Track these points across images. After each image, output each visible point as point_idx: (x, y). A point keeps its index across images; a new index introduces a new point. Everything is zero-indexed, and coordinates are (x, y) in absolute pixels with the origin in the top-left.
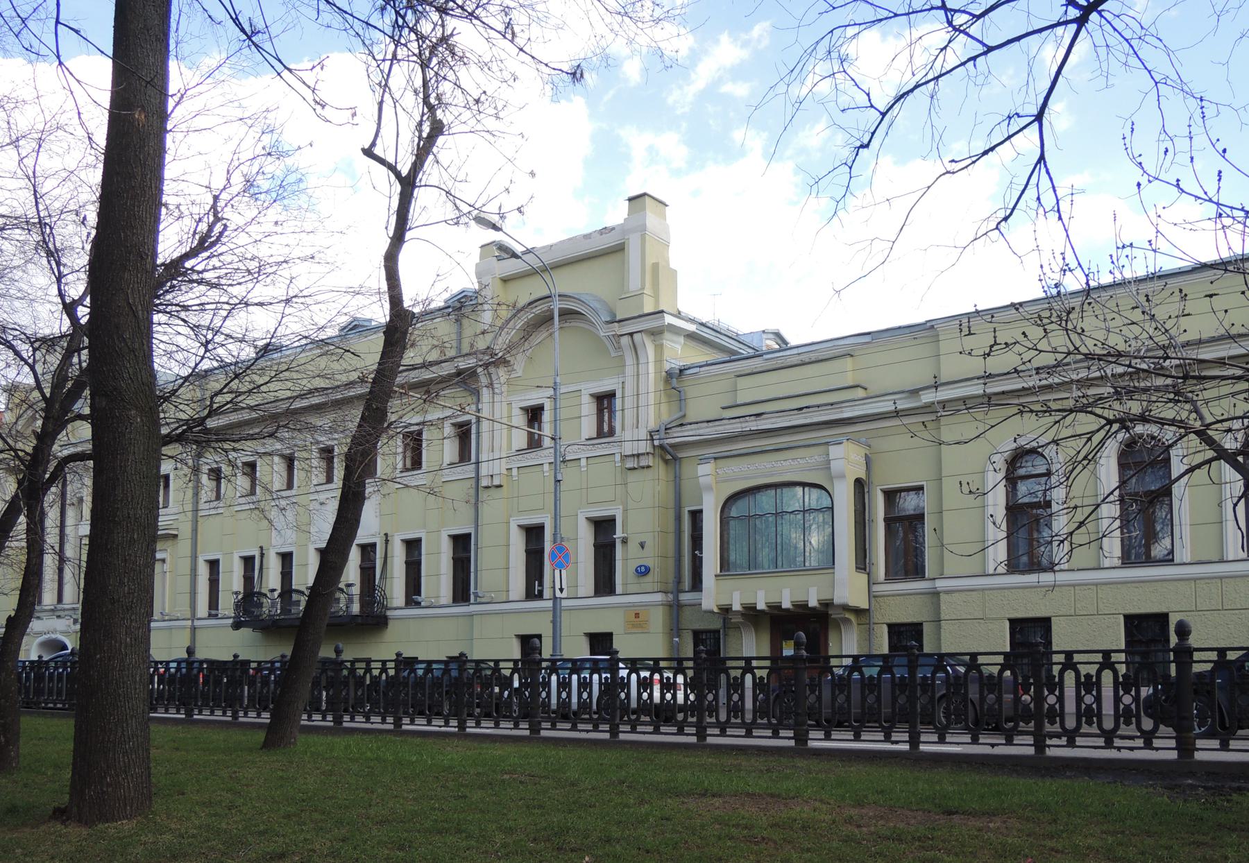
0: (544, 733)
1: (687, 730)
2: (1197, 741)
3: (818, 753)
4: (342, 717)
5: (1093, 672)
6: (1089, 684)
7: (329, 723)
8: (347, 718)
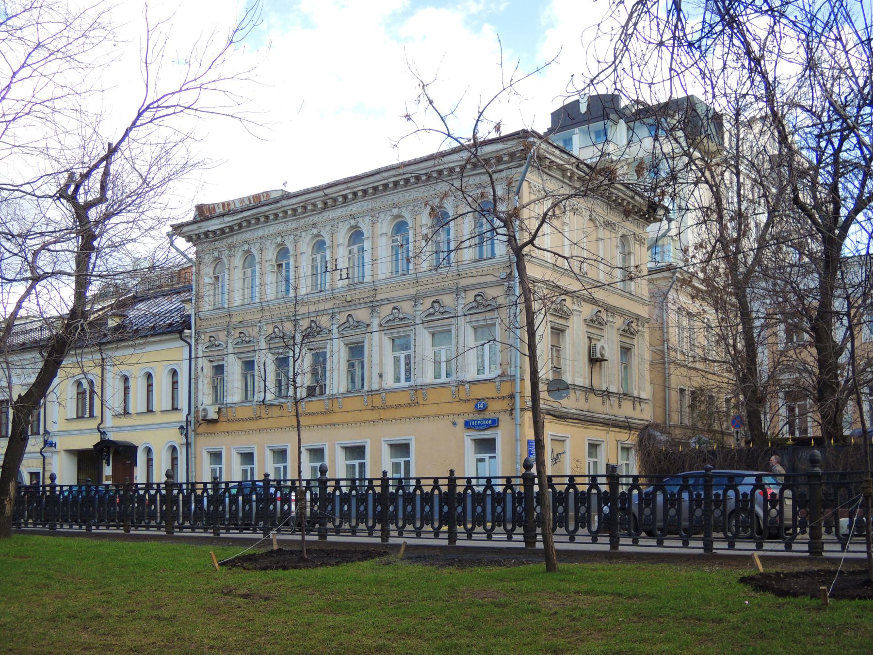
0: (132, 532)
1: (441, 536)
2: (825, 545)
3: (628, 557)
4: (55, 525)
5: (749, 492)
6: (234, 500)
7: (518, 541)
8: (94, 527)
